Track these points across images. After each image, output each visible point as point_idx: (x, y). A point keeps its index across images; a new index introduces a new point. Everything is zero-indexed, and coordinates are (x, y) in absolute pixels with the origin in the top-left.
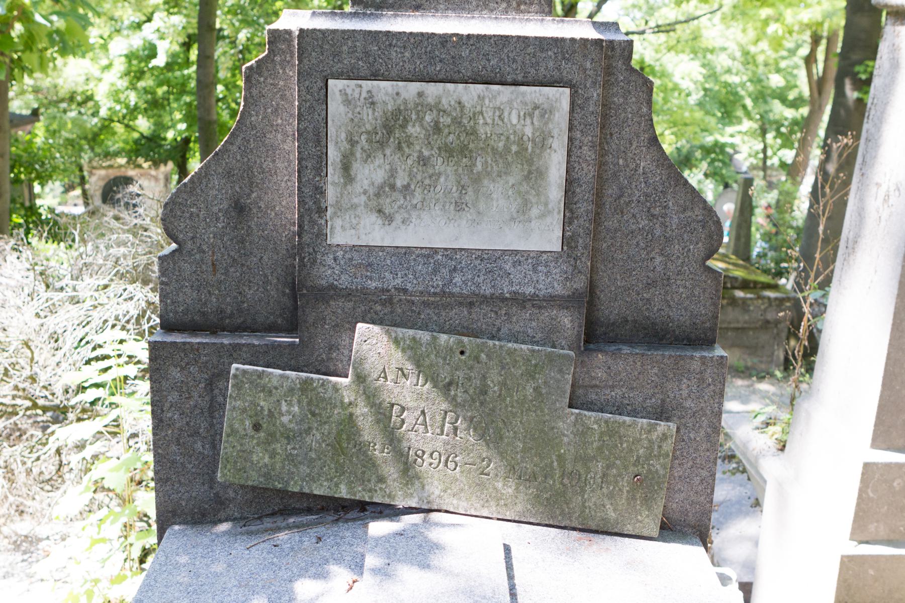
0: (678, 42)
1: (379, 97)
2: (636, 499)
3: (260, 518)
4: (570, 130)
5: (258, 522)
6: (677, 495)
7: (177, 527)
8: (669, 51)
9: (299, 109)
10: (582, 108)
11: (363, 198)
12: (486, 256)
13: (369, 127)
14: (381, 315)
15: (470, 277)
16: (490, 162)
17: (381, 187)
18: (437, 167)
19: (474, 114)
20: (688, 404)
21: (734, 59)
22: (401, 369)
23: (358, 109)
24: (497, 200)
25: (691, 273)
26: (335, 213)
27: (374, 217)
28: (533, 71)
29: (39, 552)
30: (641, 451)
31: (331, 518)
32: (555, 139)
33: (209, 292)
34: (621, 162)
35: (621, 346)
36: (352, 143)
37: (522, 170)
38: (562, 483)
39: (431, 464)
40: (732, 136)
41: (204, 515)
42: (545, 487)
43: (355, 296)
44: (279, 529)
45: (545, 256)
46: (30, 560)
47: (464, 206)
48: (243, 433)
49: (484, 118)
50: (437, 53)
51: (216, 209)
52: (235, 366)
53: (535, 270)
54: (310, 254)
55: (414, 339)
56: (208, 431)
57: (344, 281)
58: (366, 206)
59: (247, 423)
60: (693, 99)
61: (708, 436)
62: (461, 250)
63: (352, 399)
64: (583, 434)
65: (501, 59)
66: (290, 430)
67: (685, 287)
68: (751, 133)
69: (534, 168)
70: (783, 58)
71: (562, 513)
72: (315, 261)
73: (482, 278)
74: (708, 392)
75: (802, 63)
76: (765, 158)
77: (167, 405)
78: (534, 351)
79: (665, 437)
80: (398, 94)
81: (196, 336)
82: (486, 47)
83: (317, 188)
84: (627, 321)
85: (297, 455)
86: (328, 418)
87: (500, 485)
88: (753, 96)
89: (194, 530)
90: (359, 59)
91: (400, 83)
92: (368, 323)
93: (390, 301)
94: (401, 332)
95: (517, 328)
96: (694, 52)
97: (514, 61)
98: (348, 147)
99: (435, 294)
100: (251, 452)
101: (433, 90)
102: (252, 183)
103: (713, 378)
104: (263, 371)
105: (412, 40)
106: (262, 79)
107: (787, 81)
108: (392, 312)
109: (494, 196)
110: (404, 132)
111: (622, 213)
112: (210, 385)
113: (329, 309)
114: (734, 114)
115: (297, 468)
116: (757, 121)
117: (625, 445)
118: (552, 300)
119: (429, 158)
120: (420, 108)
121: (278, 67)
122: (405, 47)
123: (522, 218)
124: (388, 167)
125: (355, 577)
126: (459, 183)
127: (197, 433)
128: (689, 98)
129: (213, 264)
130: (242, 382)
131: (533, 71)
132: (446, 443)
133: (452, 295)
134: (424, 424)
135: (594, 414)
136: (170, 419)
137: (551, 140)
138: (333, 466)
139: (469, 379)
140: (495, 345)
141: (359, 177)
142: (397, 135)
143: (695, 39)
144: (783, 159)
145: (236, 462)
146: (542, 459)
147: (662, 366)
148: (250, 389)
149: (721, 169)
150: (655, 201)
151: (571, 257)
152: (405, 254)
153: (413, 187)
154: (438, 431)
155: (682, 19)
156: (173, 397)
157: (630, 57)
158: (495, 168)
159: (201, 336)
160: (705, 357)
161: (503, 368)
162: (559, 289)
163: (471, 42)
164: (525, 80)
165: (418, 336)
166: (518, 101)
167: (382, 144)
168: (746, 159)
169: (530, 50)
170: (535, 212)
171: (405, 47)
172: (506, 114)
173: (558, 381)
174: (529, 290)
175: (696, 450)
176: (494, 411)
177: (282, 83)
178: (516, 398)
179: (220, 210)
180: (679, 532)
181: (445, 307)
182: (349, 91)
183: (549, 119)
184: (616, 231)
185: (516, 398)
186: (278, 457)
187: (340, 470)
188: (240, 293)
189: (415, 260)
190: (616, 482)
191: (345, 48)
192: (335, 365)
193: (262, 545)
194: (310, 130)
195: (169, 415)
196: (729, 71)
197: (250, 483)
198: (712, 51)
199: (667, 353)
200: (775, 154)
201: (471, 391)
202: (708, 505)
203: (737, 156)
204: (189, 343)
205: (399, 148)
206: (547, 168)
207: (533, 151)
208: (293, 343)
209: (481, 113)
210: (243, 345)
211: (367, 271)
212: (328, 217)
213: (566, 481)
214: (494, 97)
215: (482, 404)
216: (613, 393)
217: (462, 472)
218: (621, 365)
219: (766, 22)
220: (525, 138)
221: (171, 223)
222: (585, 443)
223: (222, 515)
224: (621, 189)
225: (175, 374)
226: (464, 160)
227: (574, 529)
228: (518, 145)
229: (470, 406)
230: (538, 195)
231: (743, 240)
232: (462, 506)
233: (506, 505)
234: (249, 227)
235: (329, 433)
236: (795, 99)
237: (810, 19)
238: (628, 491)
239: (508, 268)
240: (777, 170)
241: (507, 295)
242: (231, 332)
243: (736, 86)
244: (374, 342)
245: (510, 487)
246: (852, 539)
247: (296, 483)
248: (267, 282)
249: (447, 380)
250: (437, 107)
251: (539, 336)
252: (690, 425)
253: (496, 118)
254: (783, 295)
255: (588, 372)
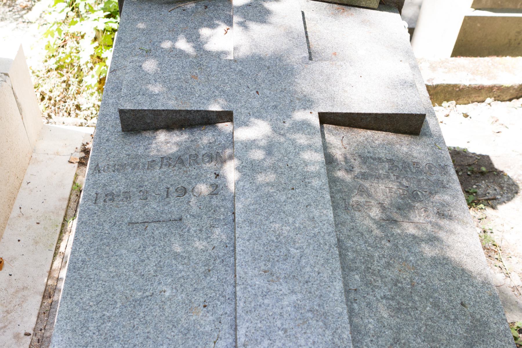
29: (18, 6)
46: (13, 10)
125: (228, 27)
180: (388, 5)
193: (177, 10)
227: (335, 3)
246: (472, 7)
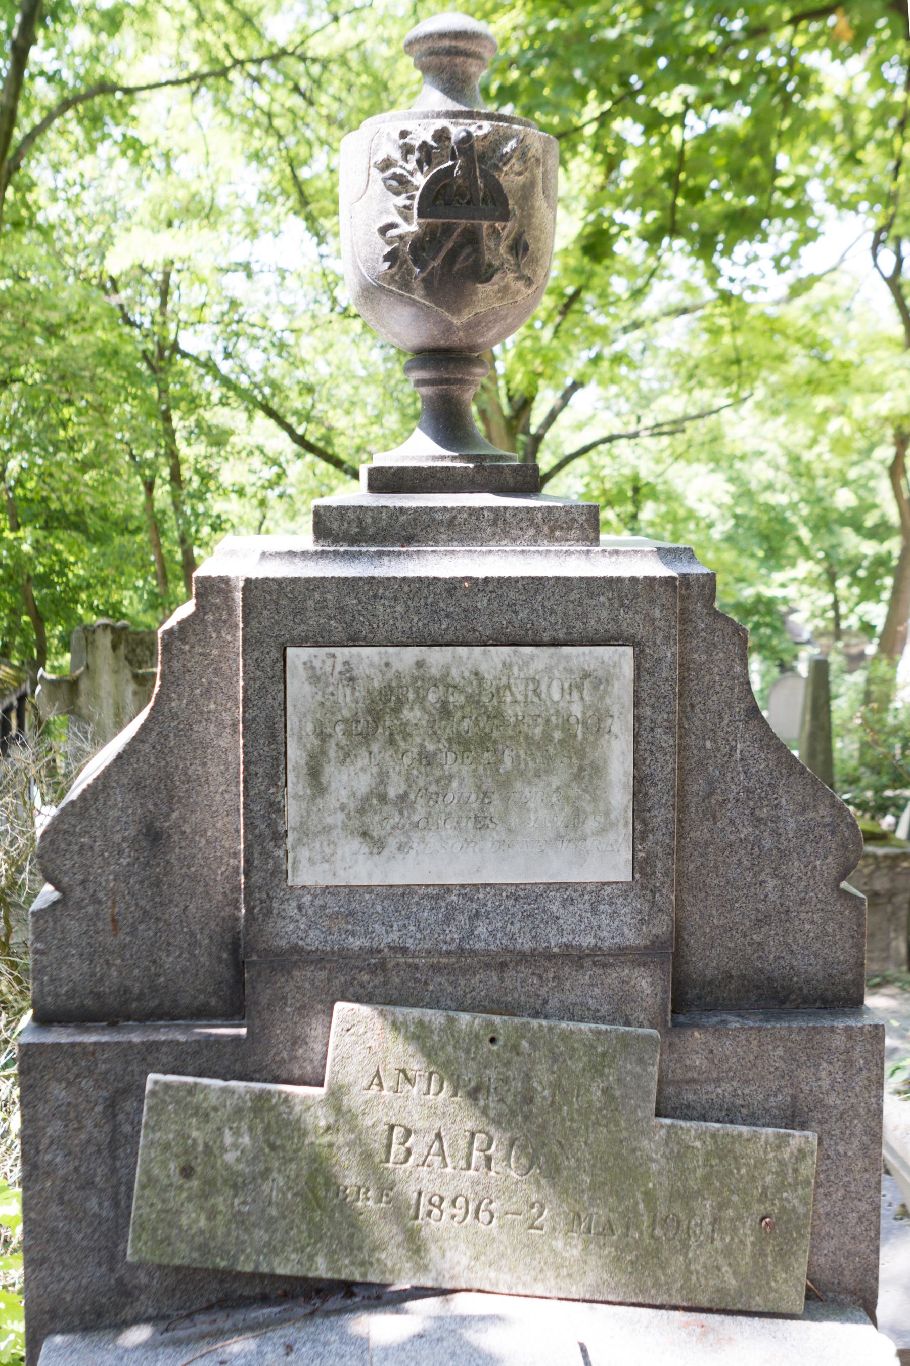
0: (689, 446)
1: (361, 670)
2: (766, 1255)
3: (189, 1316)
4: (636, 705)
5: (187, 1323)
6: (825, 1244)
7: (58, 1339)
8: (677, 459)
9: (245, 691)
10: (652, 675)
11: (340, 816)
12: (522, 894)
13: (346, 713)
14: (369, 987)
15: (499, 925)
16: (523, 756)
17: (366, 799)
18: (447, 767)
19: (498, 689)
20: (832, 1100)
21: (777, 468)
22: (403, 1071)
23: (331, 689)
24: (536, 811)
25: (820, 901)
26: (299, 840)
27: (356, 844)
28: (579, 625)
30: (769, 1179)
31: (301, 1311)
32: (616, 719)
33: (107, 962)
34: (708, 744)
35: (725, 1017)
36: (323, 737)
37: (570, 766)
38: (652, 1236)
39: (453, 1217)
40: (783, 586)
41: (99, 1315)
42: (628, 1245)
43: (329, 961)
44: (221, 1334)
45: (608, 890)
47: (488, 821)
48: (166, 1182)
49: (512, 694)
50: (442, 604)
51: (117, 838)
52: (152, 1077)
53: (595, 911)
54: (262, 902)
55: (421, 1023)
56: (107, 1180)
57: (314, 940)
58: (345, 827)
59: (172, 1165)
60: (716, 534)
61: (864, 1148)
62: (485, 886)
63: (331, 1120)
64: (680, 1157)
65: (534, 610)
66: (239, 1174)
67: (813, 922)
68: (813, 582)
69: (587, 762)
70: (854, 464)
71: (656, 1284)
72: (270, 912)
73: (517, 925)
74: (860, 1081)
75: (885, 475)
76: (838, 618)
77: (45, 1142)
78: (599, 1032)
79: (801, 1155)
80: (387, 665)
81: (88, 1030)
82: (511, 595)
83: (271, 805)
84: (731, 977)
85: (249, 1213)
86: (297, 1151)
87: (559, 1244)
88: (811, 524)
89: (87, 1340)
90: (330, 618)
91: (391, 650)
92: (349, 1001)
93: (382, 966)
94: (401, 1012)
95: (572, 998)
96: (716, 460)
97: (552, 612)
98: (317, 742)
99: (449, 953)
100: (178, 1213)
101: (437, 657)
102: (172, 797)
103: (865, 1059)
104: (196, 1084)
105: (406, 589)
106: (187, 647)
107: (861, 499)
108: (385, 983)
109: (531, 805)
110: (398, 719)
111: (714, 817)
112: (112, 1106)
113: (292, 983)
114: (783, 552)
115: (250, 1234)
116: (819, 561)
117: (743, 1171)
118: (621, 953)
119: (435, 754)
120: (419, 683)
121: (210, 629)
122: (396, 598)
123: (572, 835)
124: (375, 770)
126: (479, 788)
127: (89, 1184)
128: (712, 531)
129: (114, 921)
130: (164, 1102)
131: (579, 625)
132: (475, 1183)
133: (474, 953)
134: (441, 1153)
135: (693, 1124)
136: (49, 1163)
137: (610, 721)
138: (304, 1227)
139: (506, 1080)
140: (541, 1026)
141: (333, 786)
142: (387, 724)
143: (714, 440)
144: (865, 619)
145: (155, 1230)
146: (620, 1199)
147: (789, 1044)
148: (175, 1112)
149: (770, 638)
150: (760, 798)
151: (646, 888)
152: (403, 895)
153: (412, 797)
154: (462, 1163)
155: (693, 412)
156: (55, 1128)
157: (712, 597)
158: (531, 764)
159: (96, 1030)
160: (851, 1028)
161: (555, 1061)
162: (631, 938)
163: (491, 588)
164: (569, 638)
165: (427, 1019)
166: (561, 668)
167: (366, 737)
168: (807, 621)
169: (574, 595)
170: (591, 825)
171: (396, 598)
172: (543, 687)
173: (638, 1077)
174: (588, 941)
175: (849, 1171)
176: (544, 1128)
177: (215, 652)
178: (576, 1106)
179: (124, 839)
180: (833, 1300)
181: (464, 971)
182: (317, 664)
183: (605, 691)
184: (707, 845)
185: (576, 1106)
186: (220, 1217)
187: (316, 1233)
188: (154, 962)
189: (417, 903)
190: (735, 1230)
191: (310, 603)
192: (301, 1067)
194: (261, 720)
195: (48, 1157)
196: (770, 487)
197: (177, 1262)
198: (742, 458)
199: (794, 1025)
200: (852, 610)
201: (509, 1099)
202: (873, 1257)
203: (793, 618)
204: (80, 1044)
205: (392, 741)
206: (605, 762)
207: (584, 738)
208: (237, 1038)
209: (508, 687)
210: (163, 1043)
211: (348, 923)
212: (289, 847)
213: (658, 1232)
214: (526, 664)
215: (526, 1118)
216: (719, 1090)
217: (501, 1227)
218: (728, 1046)
219: (825, 415)
220: (573, 720)
221: (51, 860)
222: (683, 1172)
223: (128, 1313)
224: (710, 783)
225: (59, 1092)
226: (486, 755)
227: (675, 1308)
228: (563, 730)
229: (509, 1122)
230: (594, 800)
231: (820, 758)
232: (504, 1280)
233: (570, 1275)
234: (168, 862)
235: (297, 1176)
236: (876, 526)
237: (891, 409)
238: (753, 1244)
239: (555, 909)
240: (857, 636)
241: (556, 950)
242: (139, 1020)
243: (784, 509)
244: (362, 1030)
245: (576, 1246)
247: (248, 1257)
248: (194, 943)
249: (473, 1084)
250: (444, 681)
251: (605, 1008)
252: (837, 1132)
253: (530, 693)
254: (898, 851)
255: (680, 1060)
